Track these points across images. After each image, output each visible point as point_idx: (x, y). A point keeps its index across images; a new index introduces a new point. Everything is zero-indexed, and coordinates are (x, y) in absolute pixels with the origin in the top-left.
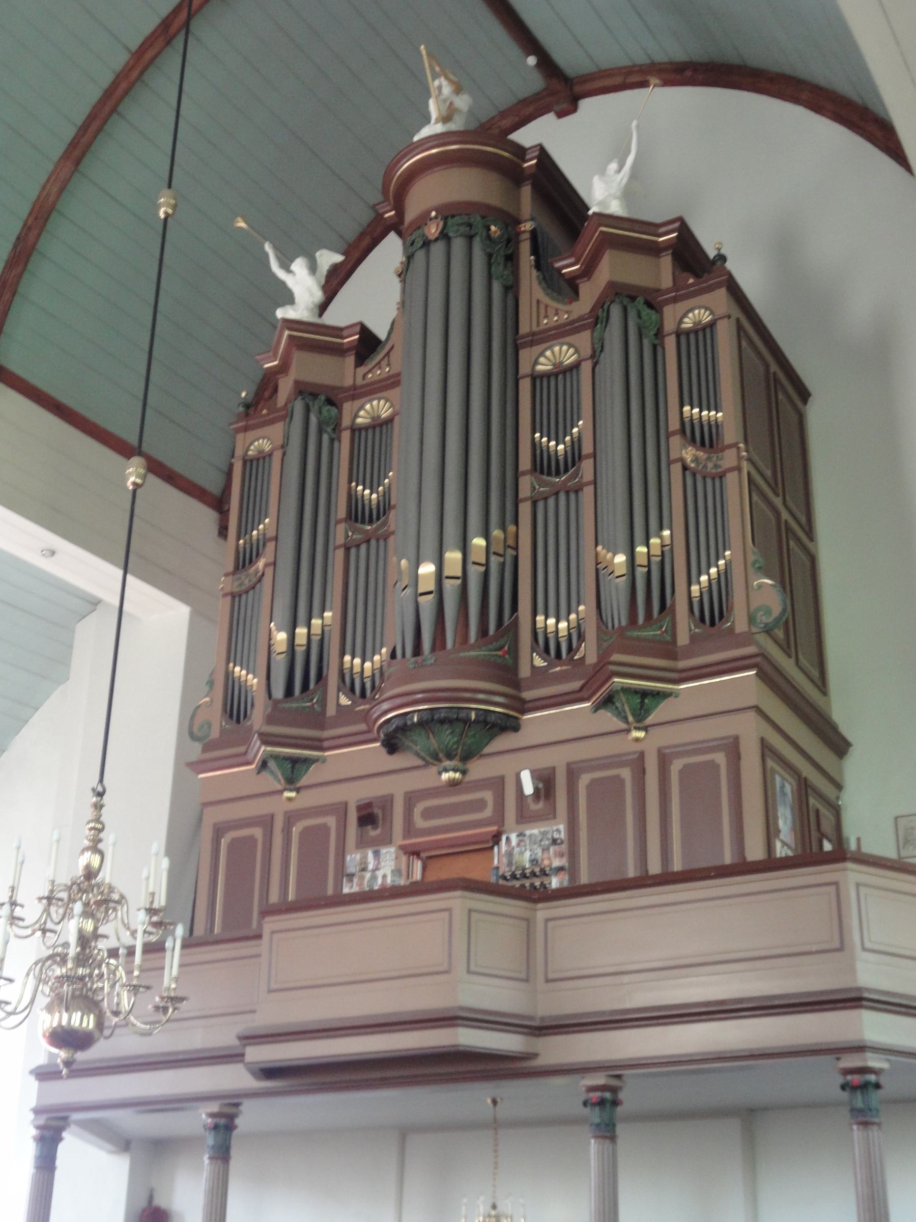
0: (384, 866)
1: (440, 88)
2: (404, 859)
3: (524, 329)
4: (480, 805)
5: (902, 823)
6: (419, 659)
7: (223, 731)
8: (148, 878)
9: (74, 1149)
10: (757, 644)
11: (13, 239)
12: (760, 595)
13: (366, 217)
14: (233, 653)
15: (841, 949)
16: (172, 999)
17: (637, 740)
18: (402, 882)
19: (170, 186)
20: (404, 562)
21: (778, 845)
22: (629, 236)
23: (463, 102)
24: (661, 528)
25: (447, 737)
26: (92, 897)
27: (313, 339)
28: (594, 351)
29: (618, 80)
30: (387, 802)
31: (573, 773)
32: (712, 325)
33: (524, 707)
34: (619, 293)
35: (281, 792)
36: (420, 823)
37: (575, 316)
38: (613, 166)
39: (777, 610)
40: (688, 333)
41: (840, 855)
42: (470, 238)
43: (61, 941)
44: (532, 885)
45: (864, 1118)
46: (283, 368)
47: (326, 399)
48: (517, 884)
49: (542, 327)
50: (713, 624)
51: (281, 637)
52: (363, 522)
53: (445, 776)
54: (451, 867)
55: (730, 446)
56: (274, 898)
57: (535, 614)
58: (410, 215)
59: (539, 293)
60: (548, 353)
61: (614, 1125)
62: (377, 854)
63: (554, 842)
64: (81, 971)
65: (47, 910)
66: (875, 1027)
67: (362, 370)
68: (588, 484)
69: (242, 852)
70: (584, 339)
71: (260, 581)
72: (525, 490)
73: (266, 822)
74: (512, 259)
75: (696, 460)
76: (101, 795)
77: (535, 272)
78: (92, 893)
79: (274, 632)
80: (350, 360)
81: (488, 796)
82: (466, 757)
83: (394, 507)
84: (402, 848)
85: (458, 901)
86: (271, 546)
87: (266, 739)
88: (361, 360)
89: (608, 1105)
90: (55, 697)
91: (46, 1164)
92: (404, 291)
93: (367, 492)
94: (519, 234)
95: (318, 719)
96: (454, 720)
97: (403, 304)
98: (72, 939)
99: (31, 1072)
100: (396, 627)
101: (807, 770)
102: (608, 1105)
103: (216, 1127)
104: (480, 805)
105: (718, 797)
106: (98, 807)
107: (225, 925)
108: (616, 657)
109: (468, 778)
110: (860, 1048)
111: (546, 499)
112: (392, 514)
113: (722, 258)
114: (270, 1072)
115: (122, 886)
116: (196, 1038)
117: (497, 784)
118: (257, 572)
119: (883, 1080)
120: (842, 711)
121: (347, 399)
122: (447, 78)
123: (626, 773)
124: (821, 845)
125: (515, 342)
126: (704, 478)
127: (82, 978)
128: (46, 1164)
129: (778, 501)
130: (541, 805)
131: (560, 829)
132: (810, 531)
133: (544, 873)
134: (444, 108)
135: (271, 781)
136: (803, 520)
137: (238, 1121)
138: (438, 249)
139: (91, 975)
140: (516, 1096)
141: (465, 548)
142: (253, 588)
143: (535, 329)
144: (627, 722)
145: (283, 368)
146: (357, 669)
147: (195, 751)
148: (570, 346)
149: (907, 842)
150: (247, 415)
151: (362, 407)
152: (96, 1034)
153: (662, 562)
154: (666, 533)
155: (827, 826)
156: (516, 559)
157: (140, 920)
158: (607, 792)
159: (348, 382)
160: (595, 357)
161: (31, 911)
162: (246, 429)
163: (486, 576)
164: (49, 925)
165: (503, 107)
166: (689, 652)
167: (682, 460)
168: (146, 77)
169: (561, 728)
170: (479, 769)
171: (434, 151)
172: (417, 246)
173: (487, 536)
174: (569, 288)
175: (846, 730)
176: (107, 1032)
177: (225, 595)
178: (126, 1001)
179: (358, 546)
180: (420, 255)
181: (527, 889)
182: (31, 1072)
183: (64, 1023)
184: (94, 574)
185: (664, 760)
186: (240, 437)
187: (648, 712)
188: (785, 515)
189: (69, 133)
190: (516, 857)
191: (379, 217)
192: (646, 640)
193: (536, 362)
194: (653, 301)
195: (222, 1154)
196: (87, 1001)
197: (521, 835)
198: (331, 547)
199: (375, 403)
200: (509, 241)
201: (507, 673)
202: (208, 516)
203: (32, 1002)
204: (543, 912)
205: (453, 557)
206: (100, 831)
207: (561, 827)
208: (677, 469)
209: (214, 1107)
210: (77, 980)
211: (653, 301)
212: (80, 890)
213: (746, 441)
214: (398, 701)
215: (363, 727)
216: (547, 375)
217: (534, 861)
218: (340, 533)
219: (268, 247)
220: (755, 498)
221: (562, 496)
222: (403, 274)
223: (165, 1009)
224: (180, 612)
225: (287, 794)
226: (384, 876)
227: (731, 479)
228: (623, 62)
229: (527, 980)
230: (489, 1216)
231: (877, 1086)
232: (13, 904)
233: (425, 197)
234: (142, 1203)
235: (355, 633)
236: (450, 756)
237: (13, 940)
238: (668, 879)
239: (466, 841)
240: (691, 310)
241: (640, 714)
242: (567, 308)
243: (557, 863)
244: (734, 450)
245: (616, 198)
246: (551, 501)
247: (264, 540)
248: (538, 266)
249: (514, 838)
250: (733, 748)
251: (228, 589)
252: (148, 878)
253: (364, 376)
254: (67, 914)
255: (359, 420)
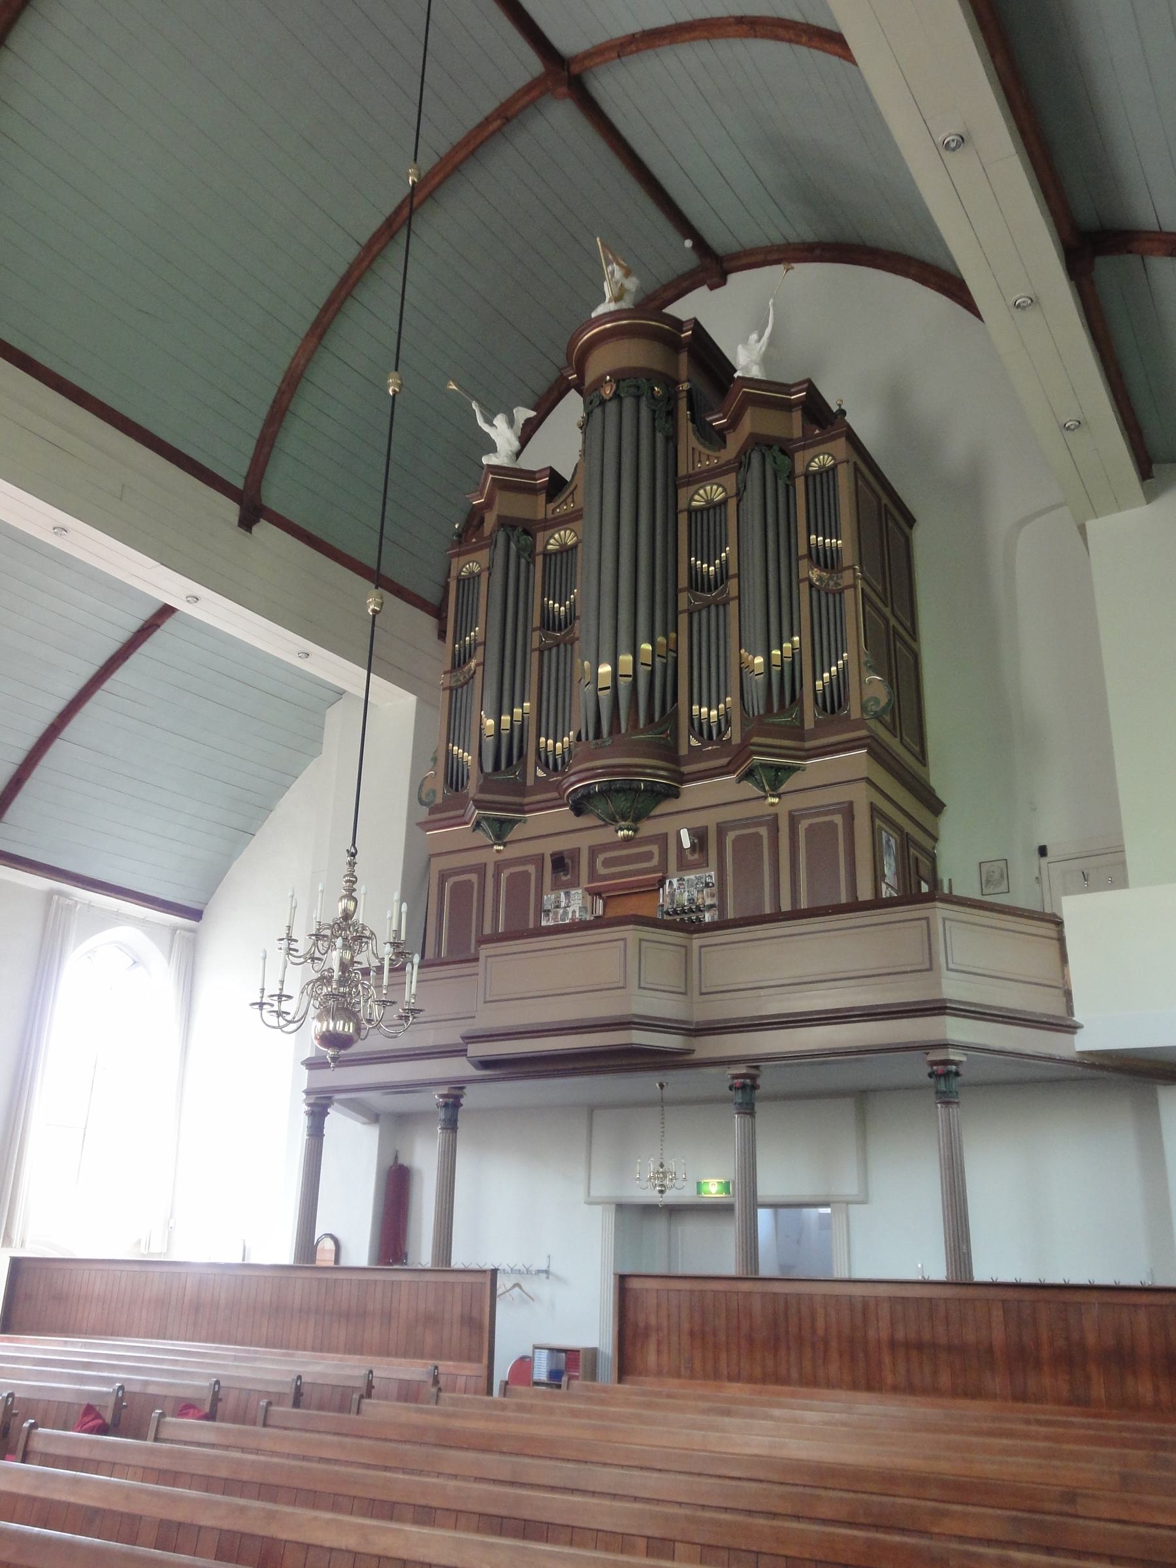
0: (573, 904)
1: (613, 273)
2: (589, 898)
3: (682, 471)
4: (648, 856)
5: (985, 867)
6: (599, 741)
7: (445, 797)
8: (391, 918)
9: (337, 1122)
10: (869, 729)
11: (270, 402)
12: (872, 687)
13: (553, 375)
14: (450, 738)
15: (930, 969)
16: (412, 1010)
17: (772, 804)
18: (589, 917)
19: (396, 369)
20: (586, 663)
21: (884, 886)
22: (769, 395)
23: (632, 284)
24: (792, 635)
25: (623, 803)
26: (351, 934)
27: (512, 481)
28: (738, 489)
29: (760, 258)
30: (575, 853)
31: (722, 830)
32: (834, 468)
33: (683, 779)
34: (759, 442)
35: (492, 846)
36: (602, 871)
37: (722, 461)
38: (754, 337)
39: (884, 701)
40: (814, 474)
41: (930, 898)
42: (638, 398)
43: (326, 967)
44: (690, 919)
45: (947, 1099)
46: (488, 505)
47: (522, 530)
48: (678, 918)
49: (697, 470)
50: (833, 712)
51: (490, 722)
52: (554, 630)
53: (621, 833)
54: (626, 905)
55: (848, 568)
56: (487, 930)
57: (691, 704)
58: (589, 378)
59: (694, 442)
60: (702, 492)
61: (753, 1105)
62: (567, 894)
63: (707, 885)
64: (342, 990)
65: (315, 945)
66: (956, 1030)
67: (551, 506)
68: (733, 599)
69: (461, 893)
70: (730, 480)
71: (472, 677)
72: (683, 604)
73: (481, 870)
74: (672, 414)
75: (820, 579)
76: (353, 855)
77: (690, 424)
78: (348, 929)
79: (484, 719)
80: (542, 498)
81: (655, 849)
82: (637, 819)
83: (578, 618)
84: (587, 890)
85: (631, 933)
86: (480, 649)
87: (479, 805)
88: (550, 498)
89: (748, 1089)
90: (312, 766)
91: (316, 1132)
92: (584, 442)
93: (557, 605)
94: (678, 392)
95: (520, 789)
96: (630, 790)
97: (584, 453)
98: (336, 967)
99: (302, 1063)
100: (581, 717)
101: (909, 827)
102: (748, 1089)
103: (446, 1105)
104: (648, 856)
105: (837, 852)
106: (352, 864)
107: (450, 951)
108: (755, 740)
109: (638, 836)
110: (944, 1045)
111: (700, 611)
112: (577, 623)
113: (843, 413)
114: (486, 1064)
115: (372, 925)
116: (429, 1037)
117: (662, 840)
118: (470, 669)
119: (962, 1070)
120: (938, 779)
121: (540, 530)
122: (618, 264)
123: (763, 831)
124: (919, 884)
125: (675, 482)
126: (827, 594)
127: (343, 995)
128: (316, 1132)
129: (887, 611)
130: (696, 856)
131: (711, 875)
132: (914, 633)
133: (699, 909)
134: (616, 291)
135: (483, 837)
136: (908, 624)
137: (462, 1101)
138: (612, 407)
139: (350, 994)
140: (678, 1082)
141: (635, 652)
142: (467, 683)
143: (691, 471)
144: (765, 791)
145: (488, 505)
146: (550, 748)
147: (423, 813)
148: (719, 485)
149: (988, 882)
150: (460, 542)
151: (552, 537)
152: (355, 1037)
153: (793, 662)
154: (796, 639)
155: (924, 870)
156: (676, 659)
157: (387, 951)
158: (748, 847)
159: (541, 516)
160: (739, 495)
161: (303, 945)
162: (458, 555)
163: (652, 674)
164: (317, 955)
165: (665, 281)
166: (814, 735)
167: (809, 579)
168: (375, 266)
169: (713, 796)
170: (648, 828)
171: (608, 325)
172: (594, 404)
173: (652, 642)
174: (715, 438)
175: (941, 794)
176: (363, 1033)
177: (444, 689)
178: (377, 1012)
179: (550, 649)
180: (598, 412)
181: (685, 923)
182: (302, 1063)
183: (331, 1028)
184: (344, 673)
185: (793, 820)
186: (454, 561)
187: (781, 783)
188: (893, 622)
189: (313, 314)
190: (677, 897)
191: (562, 378)
192: (779, 725)
193: (692, 499)
194: (786, 449)
195: (451, 1125)
196: (349, 1013)
197: (681, 879)
198: (528, 651)
199: (562, 533)
200: (669, 399)
201: (669, 752)
202: (428, 623)
203: (306, 1013)
204: (697, 941)
205: (626, 659)
206: (354, 883)
207: (713, 873)
208: (804, 587)
209: (444, 1090)
210: (338, 996)
211: (786, 449)
212: (340, 928)
213: (861, 565)
214: (583, 775)
215: (555, 794)
216: (700, 510)
217: (691, 901)
218: (535, 639)
219: (474, 405)
220: (868, 608)
221: (713, 608)
222: (584, 426)
223: (407, 1018)
224: (410, 700)
225: (496, 847)
226: (574, 912)
227: (849, 594)
228: (765, 242)
229: (685, 994)
230: (658, 1173)
231: (957, 1074)
232: (290, 939)
233: (601, 363)
234: (390, 1162)
235: (551, 717)
236: (624, 818)
237: (289, 964)
238: (797, 914)
239: (639, 884)
240: (817, 456)
241: (775, 787)
242: (717, 454)
243: (709, 902)
244: (851, 571)
245: (756, 363)
246: (704, 613)
247: (475, 644)
248: (693, 420)
249: (675, 881)
250: (848, 811)
251: (447, 684)
252: (391, 918)
253: (554, 510)
254: (331, 946)
255: (550, 547)
